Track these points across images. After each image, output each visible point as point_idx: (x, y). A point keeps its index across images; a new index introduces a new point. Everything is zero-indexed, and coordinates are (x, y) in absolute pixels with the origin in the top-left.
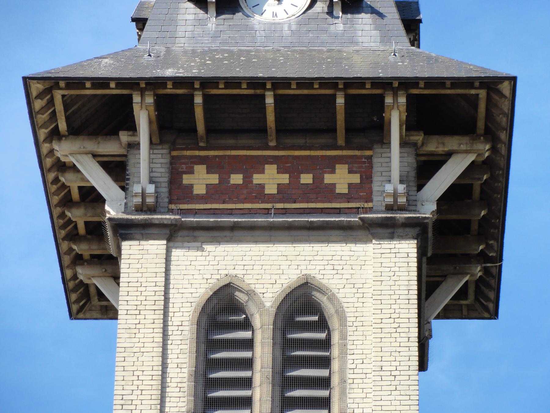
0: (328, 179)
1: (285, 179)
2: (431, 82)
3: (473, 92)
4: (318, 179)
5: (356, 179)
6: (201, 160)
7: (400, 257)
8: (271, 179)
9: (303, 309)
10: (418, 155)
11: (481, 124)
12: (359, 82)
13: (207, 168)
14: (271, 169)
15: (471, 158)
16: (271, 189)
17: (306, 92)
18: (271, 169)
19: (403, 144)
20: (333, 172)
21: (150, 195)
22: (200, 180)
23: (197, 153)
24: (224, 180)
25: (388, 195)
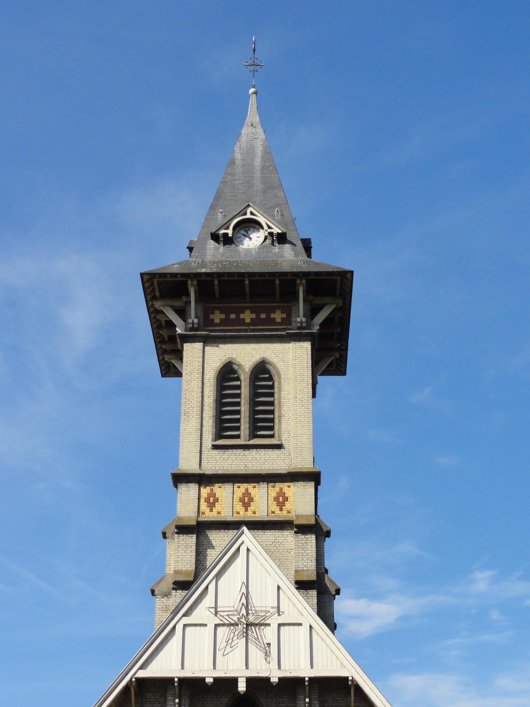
0: (272, 316)
1: (254, 316)
5: (284, 316)
9: (262, 371)
11: (338, 291)
14: (217, 313)
15: (334, 306)
21: (196, 324)
22: (217, 317)
24: (228, 316)
25: (299, 322)
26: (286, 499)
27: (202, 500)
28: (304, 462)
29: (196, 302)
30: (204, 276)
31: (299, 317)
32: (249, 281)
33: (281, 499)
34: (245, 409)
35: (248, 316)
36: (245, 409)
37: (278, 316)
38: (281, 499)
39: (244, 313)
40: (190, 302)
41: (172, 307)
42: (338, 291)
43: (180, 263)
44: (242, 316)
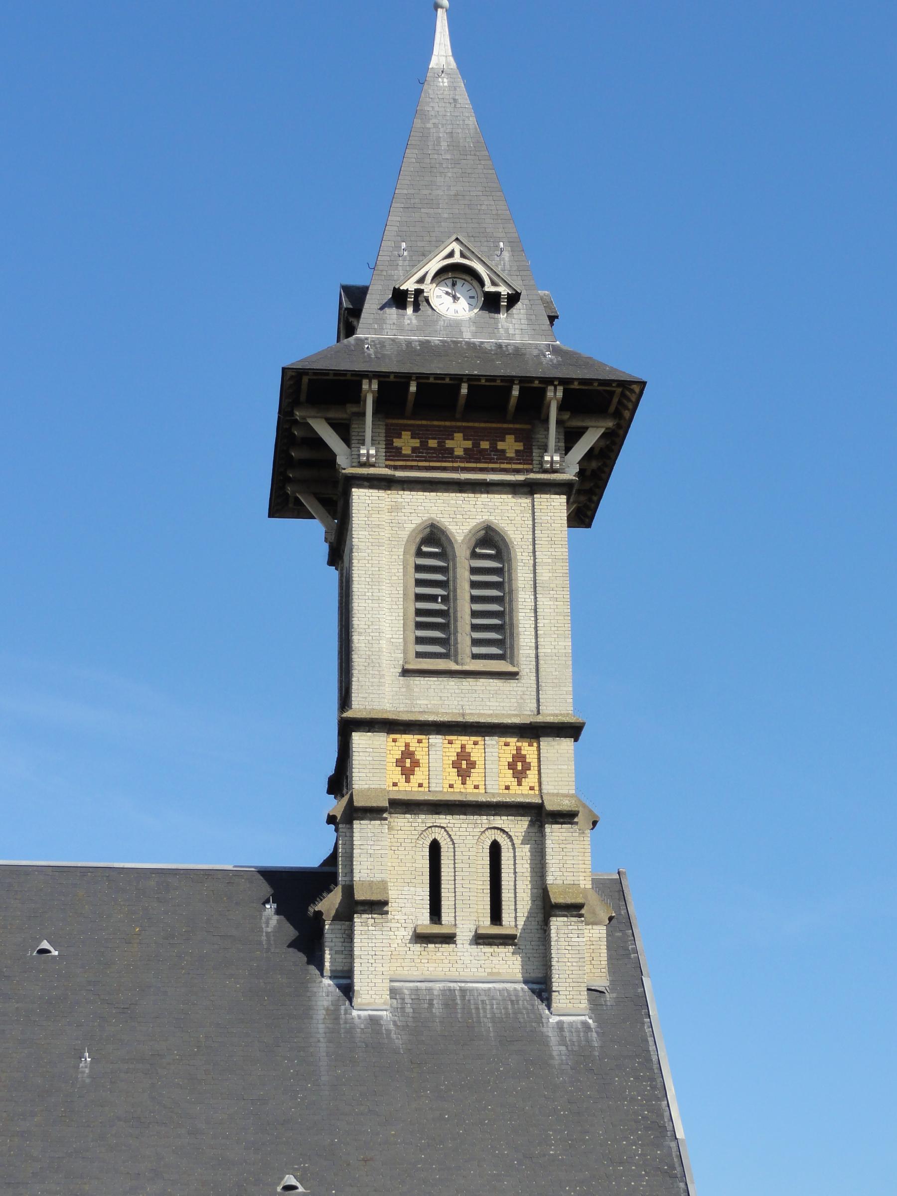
1: (469, 444)
2: (583, 381)
4: (441, 444)
6: (459, 430)
7: (555, 507)
8: (459, 444)
9: (490, 540)
12: (531, 379)
13: (516, 438)
14: (510, 439)
19: (559, 422)
20: (503, 440)
24: (476, 445)
26: (400, 763)
27: (534, 764)
28: (558, 706)
29: (375, 413)
33: (408, 763)
34: (464, 604)
35: (459, 444)
36: (464, 604)
37: (510, 445)
38: (464, 764)
40: (363, 414)
42: (612, 409)
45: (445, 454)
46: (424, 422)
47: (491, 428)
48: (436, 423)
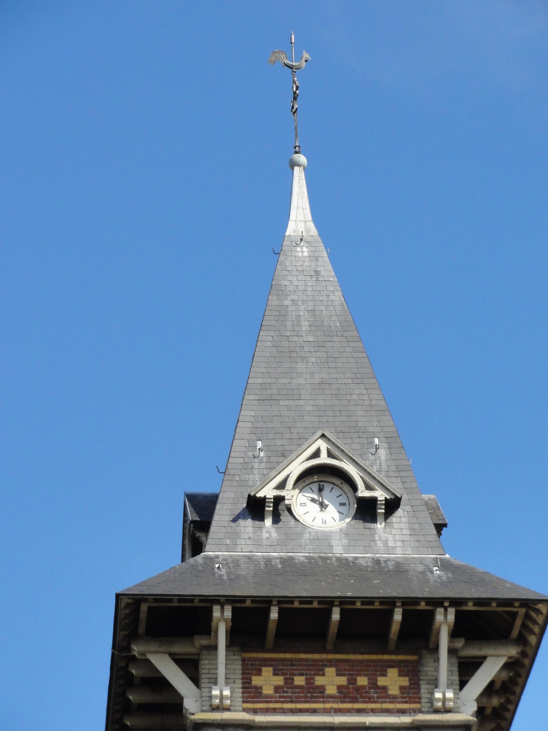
1: (343, 681)
3: (516, 610)
4: (309, 681)
6: (266, 662)
8: (331, 680)
10: (459, 658)
16: (331, 690)
17: (482, 609)
18: (330, 671)
23: (386, 657)
24: (352, 681)
29: (230, 645)
30: (494, 604)
31: (216, 683)
32: (342, 613)
37: (393, 681)
39: (385, 675)
41: (171, 655)
43: (512, 584)
44: (319, 681)
45: (315, 693)
46: (288, 656)
47: (369, 661)
48: (303, 656)
